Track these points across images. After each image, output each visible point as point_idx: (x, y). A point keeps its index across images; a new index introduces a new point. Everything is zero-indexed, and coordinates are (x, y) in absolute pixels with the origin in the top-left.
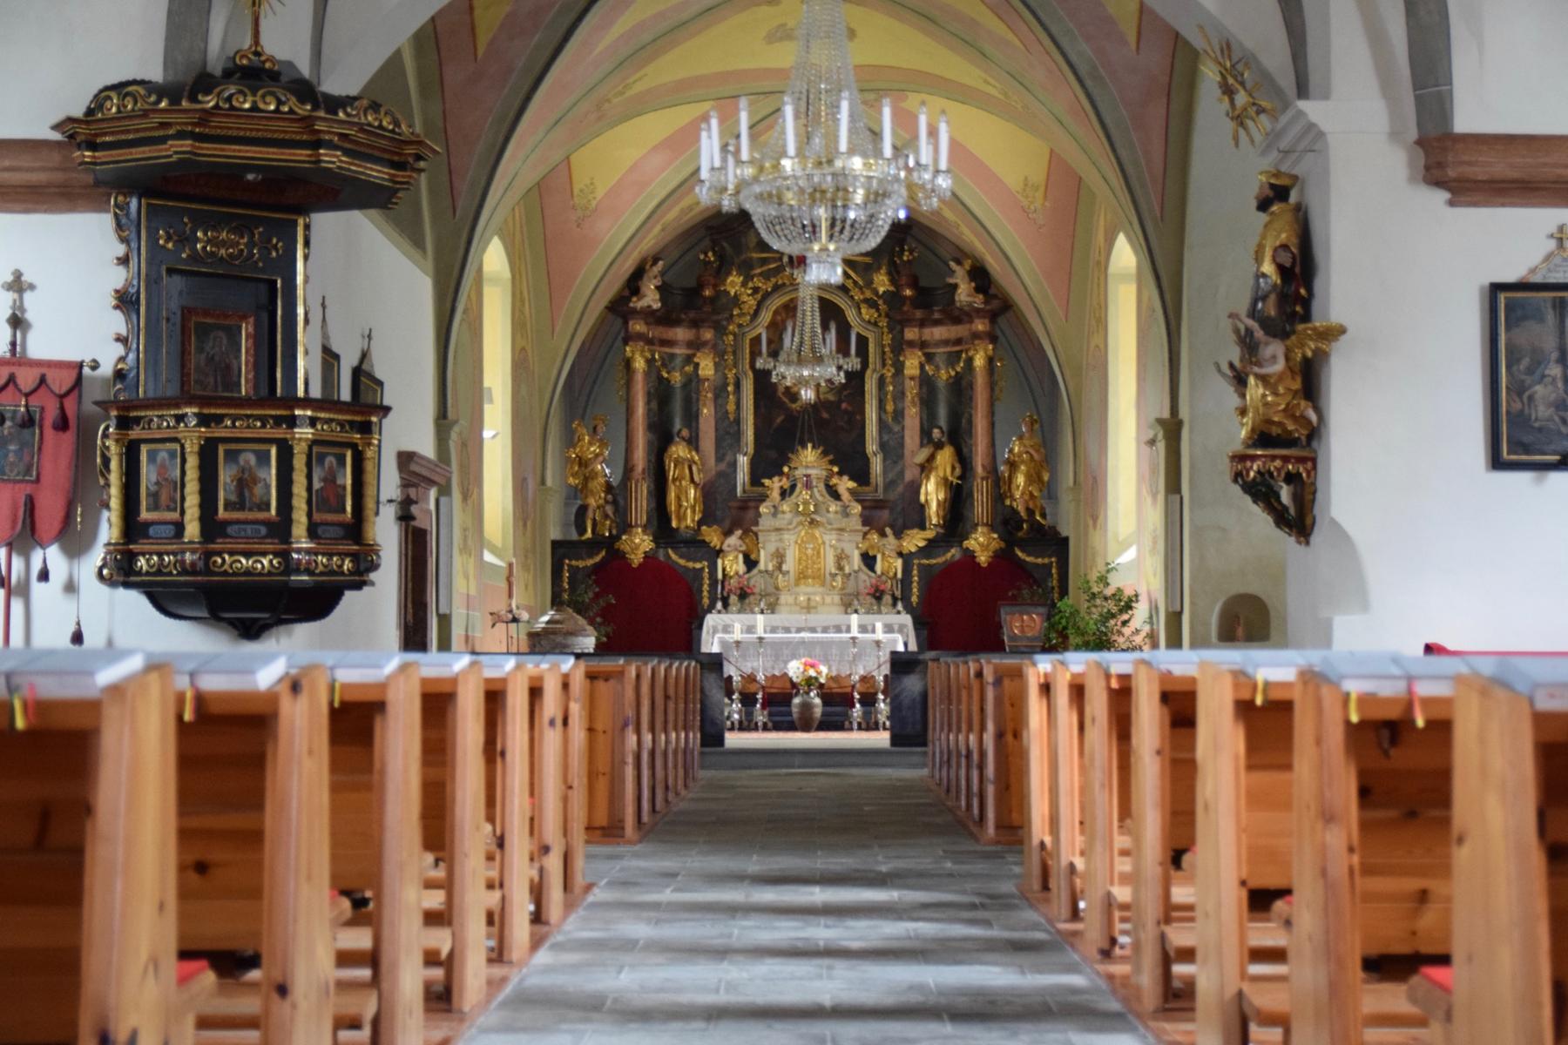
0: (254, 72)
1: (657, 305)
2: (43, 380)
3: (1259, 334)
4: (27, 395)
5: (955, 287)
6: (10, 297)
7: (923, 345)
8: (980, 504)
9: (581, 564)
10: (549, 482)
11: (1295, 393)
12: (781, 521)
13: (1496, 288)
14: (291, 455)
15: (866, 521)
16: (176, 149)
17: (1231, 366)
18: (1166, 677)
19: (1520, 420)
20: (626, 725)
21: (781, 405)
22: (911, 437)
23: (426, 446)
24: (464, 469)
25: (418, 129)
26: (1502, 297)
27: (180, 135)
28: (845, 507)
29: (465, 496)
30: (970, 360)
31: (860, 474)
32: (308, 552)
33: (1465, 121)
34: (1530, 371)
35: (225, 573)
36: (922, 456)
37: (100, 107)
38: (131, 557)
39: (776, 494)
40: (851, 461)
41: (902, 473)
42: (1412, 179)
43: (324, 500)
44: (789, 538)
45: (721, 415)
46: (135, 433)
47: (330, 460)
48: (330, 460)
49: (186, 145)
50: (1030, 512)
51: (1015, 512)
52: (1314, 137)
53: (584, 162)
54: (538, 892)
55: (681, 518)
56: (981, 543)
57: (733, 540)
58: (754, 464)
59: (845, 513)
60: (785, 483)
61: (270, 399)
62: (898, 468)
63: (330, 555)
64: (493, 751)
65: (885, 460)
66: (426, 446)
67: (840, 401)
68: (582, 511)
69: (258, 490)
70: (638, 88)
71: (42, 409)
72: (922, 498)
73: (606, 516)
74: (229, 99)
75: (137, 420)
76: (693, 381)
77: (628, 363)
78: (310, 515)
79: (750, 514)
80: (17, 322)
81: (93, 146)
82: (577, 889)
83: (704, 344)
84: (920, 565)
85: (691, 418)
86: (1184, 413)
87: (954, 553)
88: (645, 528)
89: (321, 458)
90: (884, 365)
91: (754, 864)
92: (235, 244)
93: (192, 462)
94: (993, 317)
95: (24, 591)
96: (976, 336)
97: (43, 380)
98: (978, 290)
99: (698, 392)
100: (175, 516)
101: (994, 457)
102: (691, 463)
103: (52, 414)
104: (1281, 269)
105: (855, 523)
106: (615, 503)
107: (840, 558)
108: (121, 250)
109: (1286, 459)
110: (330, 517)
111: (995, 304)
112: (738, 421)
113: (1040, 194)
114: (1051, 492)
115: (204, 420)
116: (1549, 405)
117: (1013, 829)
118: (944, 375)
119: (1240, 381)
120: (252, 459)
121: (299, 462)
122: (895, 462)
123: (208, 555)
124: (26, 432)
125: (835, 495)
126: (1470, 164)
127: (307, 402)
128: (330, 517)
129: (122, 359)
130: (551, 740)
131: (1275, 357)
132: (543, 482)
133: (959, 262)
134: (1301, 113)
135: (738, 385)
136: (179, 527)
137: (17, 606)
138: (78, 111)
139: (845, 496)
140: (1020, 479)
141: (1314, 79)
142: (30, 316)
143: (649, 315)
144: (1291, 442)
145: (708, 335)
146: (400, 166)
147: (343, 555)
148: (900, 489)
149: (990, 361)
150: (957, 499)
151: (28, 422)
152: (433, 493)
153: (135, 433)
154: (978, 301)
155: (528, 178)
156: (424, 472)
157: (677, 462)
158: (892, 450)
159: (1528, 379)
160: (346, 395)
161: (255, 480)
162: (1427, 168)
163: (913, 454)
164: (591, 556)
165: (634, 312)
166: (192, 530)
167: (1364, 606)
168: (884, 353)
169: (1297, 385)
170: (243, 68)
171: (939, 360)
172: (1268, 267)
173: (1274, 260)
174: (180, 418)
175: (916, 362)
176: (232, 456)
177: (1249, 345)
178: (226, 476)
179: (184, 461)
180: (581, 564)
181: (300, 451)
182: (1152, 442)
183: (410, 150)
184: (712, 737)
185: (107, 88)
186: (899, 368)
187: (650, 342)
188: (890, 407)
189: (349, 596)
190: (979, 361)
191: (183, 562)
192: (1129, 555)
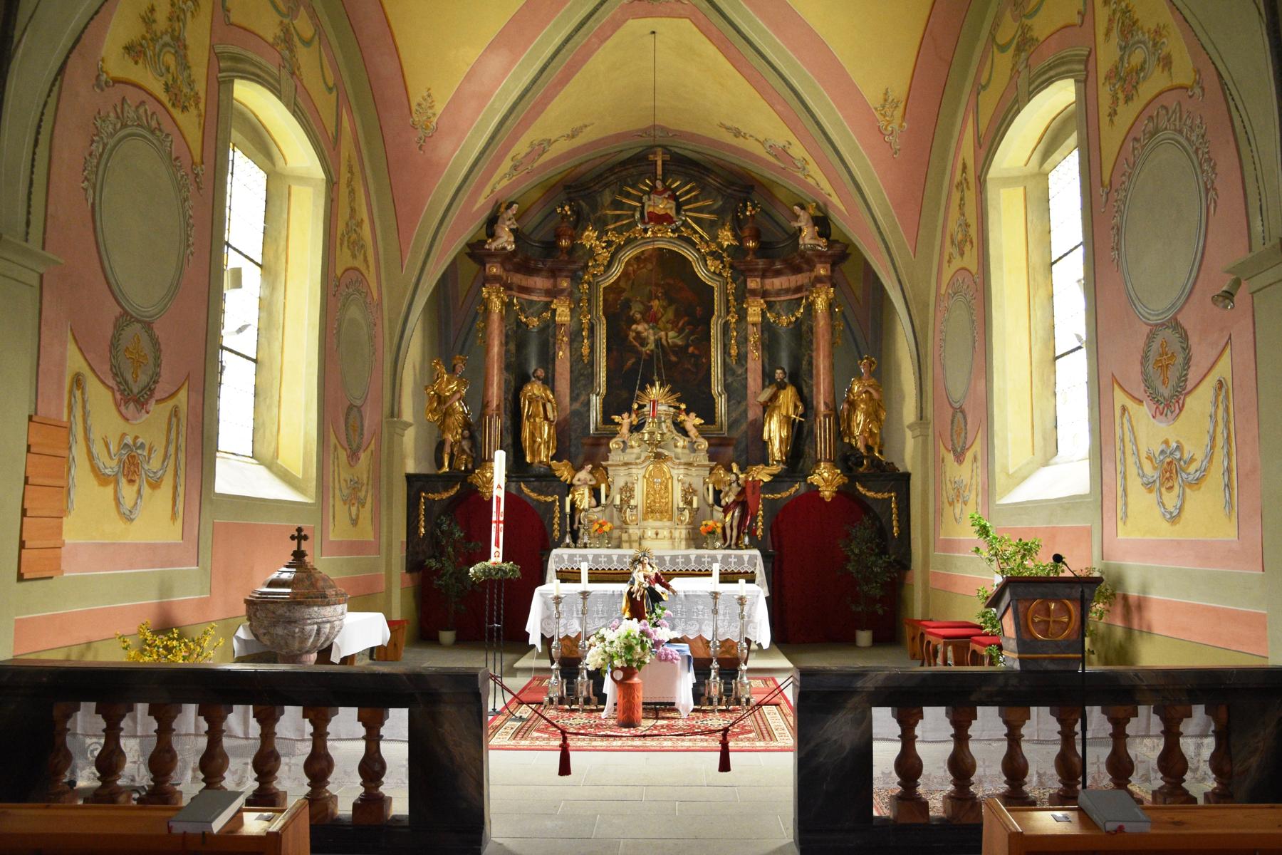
5: (800, 230)
7: (764, 294)
12: (629, 456)
21: (633, 350)
22: (754, 380)
28: (693, 443)
30: (810, 307)
36: (765, 395)
41: (745, 412)
44: (638, 472)
45: (576, 359)
50: (869, 448)
55: (535, 453)
56: (825, 478)
57: (583, 475)
59: (693, 448)
62: (742, 408)
65: (729, 400)
67: (687, 346)
72: (766, 436)
73: (463, 451)
76: (549, 328)
77: (486, 303)
79: (603, 449)
83: (562, 291)
85: (547, 359)
90: (728, 312)
96: (819, 280)
105: (703, 458)
106: (472, 438)
107: (689, 492)
111: (838, 248)
112: (591, 364)
113: (899, 113)
125: (684, 432)
133: (803, 208)
135: (592, 330)
139: (693, 432)
148: (744, 427)
149: (831, 305)
150: (799, 435)
158: (736, 392)
163: (756, 395)
164: (446, 490)
168: (728, 301)
175: (758, 310)
186: (742, 314)
188: (734, 352)
190: (821, 304)
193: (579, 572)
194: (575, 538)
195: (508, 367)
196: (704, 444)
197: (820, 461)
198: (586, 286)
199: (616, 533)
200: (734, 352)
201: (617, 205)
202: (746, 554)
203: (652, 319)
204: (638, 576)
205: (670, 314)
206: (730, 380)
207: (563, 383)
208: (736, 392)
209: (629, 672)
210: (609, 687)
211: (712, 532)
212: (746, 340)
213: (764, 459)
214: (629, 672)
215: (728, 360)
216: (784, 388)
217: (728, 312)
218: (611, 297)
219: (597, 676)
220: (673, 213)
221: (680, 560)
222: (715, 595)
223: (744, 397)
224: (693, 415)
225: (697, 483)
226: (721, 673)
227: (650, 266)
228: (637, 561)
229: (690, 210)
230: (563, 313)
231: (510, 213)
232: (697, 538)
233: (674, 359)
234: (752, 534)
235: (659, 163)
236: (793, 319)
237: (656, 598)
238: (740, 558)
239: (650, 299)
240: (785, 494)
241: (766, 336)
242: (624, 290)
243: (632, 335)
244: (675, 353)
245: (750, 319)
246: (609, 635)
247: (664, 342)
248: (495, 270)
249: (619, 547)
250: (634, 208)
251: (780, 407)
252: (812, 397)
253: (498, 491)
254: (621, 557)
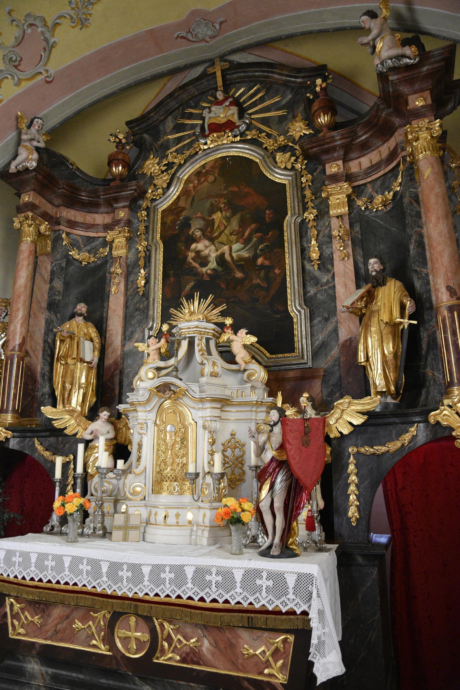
21: (192, 272)
41: (336, 331)
62: (330, 327)
67: (256, 257)
72: (361, 358)
84: (358, 455)
87: (415, 434)
112: (146, 295)
122: (327, 319)
125: (228, 356)
135: (148, 259)
139: (241, 355)
148: (335, 352)
158: (321, 307)
167: (133, 390)
168: (304, 197)
175: (343, 198)
197: (451, 384)
198: (144, 213)
201: (179, 128)
203: (209, 234)
205: (235, 224)
206: (312, 291)
213: (363, 389)
215: (308, 266)
216: (383, 283)
217: (305, 209)
218: (169, 219)
220: (235, 119)
221: (167, 576)
223: (333, 312)
224: (243, 332)
227: (211, 178)
229: (256, 113)
233: (239, 275)
235: (219, 74)
236: (390, 196)
239: (212, 211)
240: (394, 446)
241: (357, 228)
242: (184, 209)
243: (191, 255)
244: (241, 268)
245: (332, 212)
247: (227, 257)
250: (193, 127)
251: (378, 311)
252: (429, 291)
254: (76, 561)
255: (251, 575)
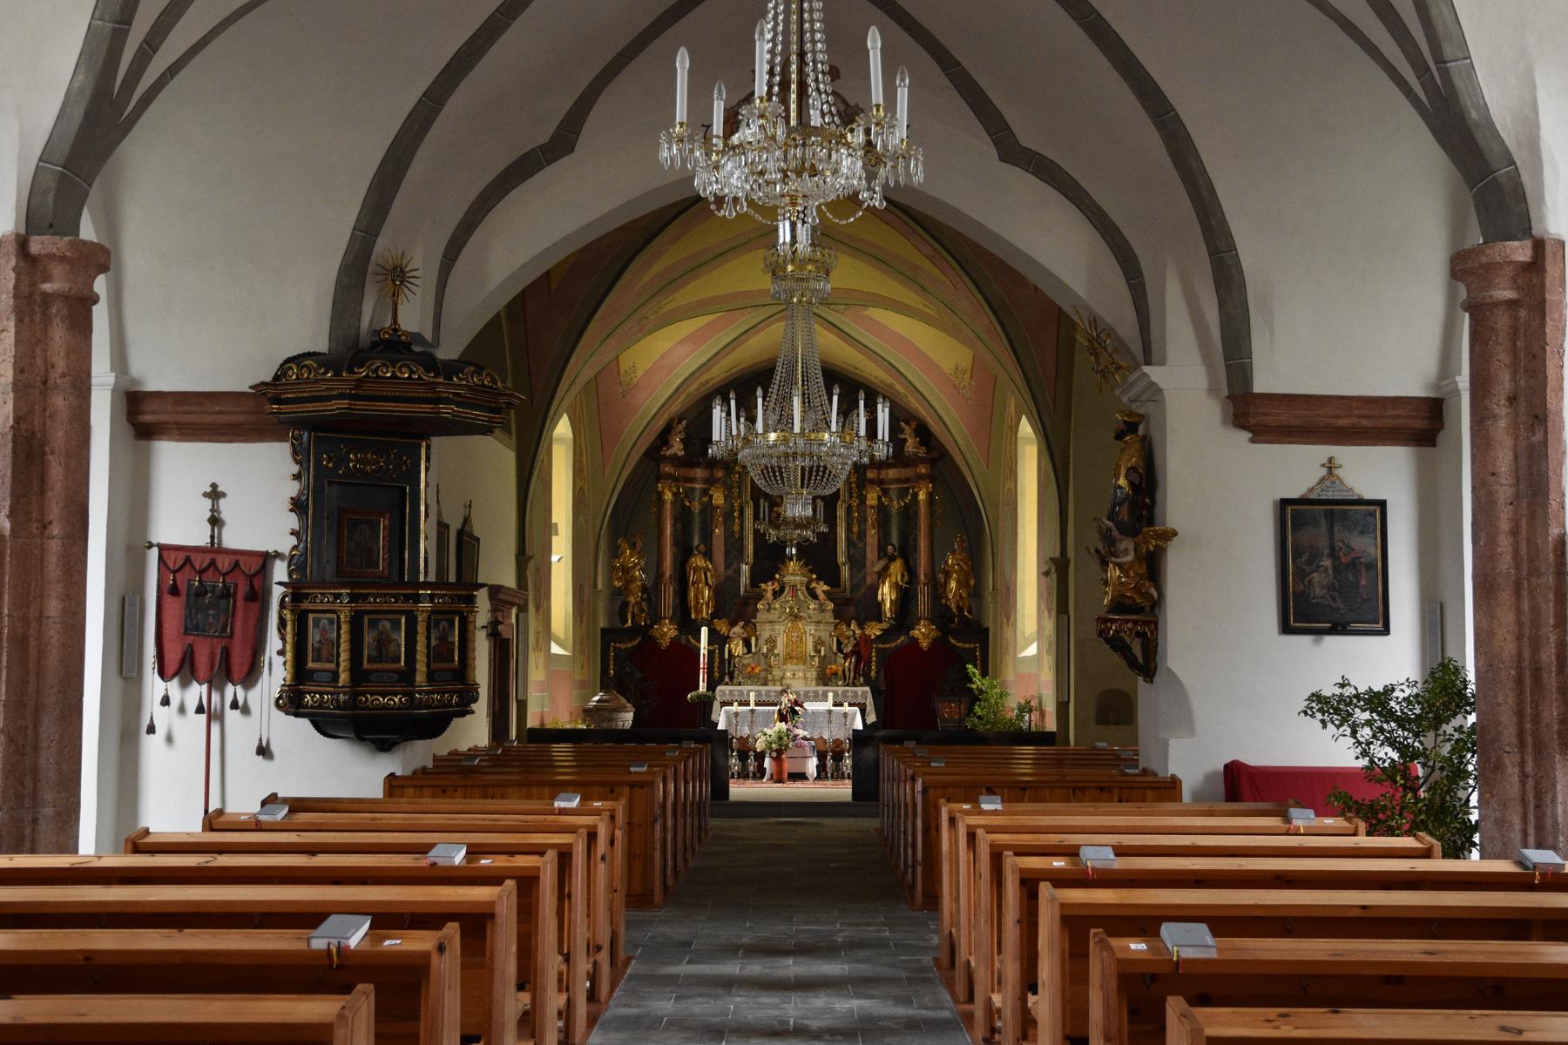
0: (394, 345)
1: (681, 453)
2: (237, 565)
3: (1116, 533)
4: (224, 575)
5: (905, 441)
6: (208, 502)
7: (880, 482)
8: (923, 603)
9: (623, 646)
10: (600, 586)
11: (1141, 576)
12: (774, 615)
13: (1284, 503)
14: (416, 622)
15: (837, 614)
16: (336, 406)
17: (1097, 551)
18: (1022, 871)
19: (1301, 597)
20: (655, 821)
22: (871, 552)
23: (509, 580)
24: (537, 590)
25: (509, 384)
26: (1289, 509)
27: (341, 396)
28: (821, 605)
29: (538, 608)
30: (915, 495)
31: (832, 577)
32: (428, 693)
33: (1261, 385)
34: (1309, 562)
35: (368, 708)
36: (878, 568)
37: (285, 374)
38: (302, 694)
39: (769, 595)
40: (828, 573)
42: (1224, 423)
43: (439, 653)
44: (780, 628)
45: (729, 534)
46: (305, 605)
47: (443, 624)
48: (443, 624)
49: (345, 403)
50: (960, 609)
51: (949, 608)
52: (1155, 391)
53: (626, 362)
54: (593, 977)
55: (699, 611)
56: (923, 632)
57: (737, 629)
58: (753, 571)
59: (822, 610)
60: (776, 586)
61: (400, 583)
63: (442, 693)
64: (563, 895)
65: (851, 568)
66: (509, 580)
68: (625, 605)
69: (392, 648)
70: (669, 307)
71: (236, 585)
73: (642, 610)
74: (376, 371)
75: (306, 596)
76: (708, 508)
77: (660, 495)
78: (428, 665)
79: (751, 608)
80: (215, 521)
81: (278, 401)
82: (620, 964)
83: (718, 480)
85: (707, 536)
86: (1071, 554)
88: (671, 619)
89: (437, 624)
90: (851, 497)
91: (746, 932)
92: (376, 462)
93: (345, 628)
94: (932, 463)
95: (220, 717)
96: (920, 477)
97: (237, 565)
98: (921, 443)
99: (712, 517)
100: (333, 666)
101: (933, 569)
102: (706, 570)
103: (242, 590)
104: (1131, 484)
105: (829, 617)
106: (649, 600)
107: (818, 643)
108: (295, 469)
109: (1136, 622)
110: (443, 665)
111: (935, 454)
112: (741, 538)
113: (968, 375)
114: (976, 593)
115: (354, 598)
116: (1323, 587)
117: (932, 901)
118: (896, 505)
119: (1104, 564)
120: (388, 625)
121: (421, 628)
123: (354, 695)
124: (223, 602)
125: (814, 596)
126: (1265, 414)
127: (426, 585)
128: (443, 665)
129: (295, 548)
130: (601, 868)
131: (1127, 550)
132: (595, 586)
133: (907, 423)
134: (1145, 375)
135: (742, 512)
136: (335, 675)
137: (215, 729)
138: (268, 378)
139: (822, 596)
140: (953, 585)
141: (1155, 356)
142: (224, 516)
143: (674, 460)
144: (1139, 610)
145: (720, 474)
146: (497, 411)
147: (451, 692)
149: (930, 495)
150: (905, 597)
151: (227, 594)
152: (514, 611)
153: (305, 605)
154: (922, 451)
155: (587, 374)
156: (509, 599)
157: (696, 570)
158: (857, 561)
159: (1308, 569)
160: (452, 578)
161: (390, 641)
162: (1235, 415)
163: (873, 565)
164: (630, 640)
165: (664, 457)
166: (344, 677)
169: (1142, 571)
170: (385, 341)
171: (893, 494)
172: (1122, 482)
173: (1126, 477)
174: (337, 596)
176: (373, 624)
177: (1107, 538)
178: (369, 638)
179: (339, 628)
180: (623, 646)
181: (421, 619)
182: (1047, 574)
183: (503, 400)
184: (721, 791)
185: (289, 360)
186: (862, 499)
187: (676, 480)
188: (855, 529)
189: (456, 721)
190: (922, 496)
191: (338, 701)
192: (1032, 650)
193: (1293, 515)
194: (732, 678)
195: (675, 543)
196: (831, 606)
199: (763, 674)
200: (855, 529)
202: (859, 690)
204: (785, 700)
207: (719, 555)
208: (857, 561)
209: (780, 752)
210: (767, 763)
211: (836, 674)
212: (865, 519)
214: (780, 752)
219: (760, 757)
222: (830, 712)
225: (825, 636)
226: (833, 758)
228: (784, 691)
230: (718, 498)
231: (681, 427)
232: (824, 679)
234: (867, 676)
237: (796, 713)
238: (855, 693)
246: (769, 731)
248: (668, 469)
249: (765, 684)
253: (704, 651)
254: (768, 692)
255: (731, 692)
